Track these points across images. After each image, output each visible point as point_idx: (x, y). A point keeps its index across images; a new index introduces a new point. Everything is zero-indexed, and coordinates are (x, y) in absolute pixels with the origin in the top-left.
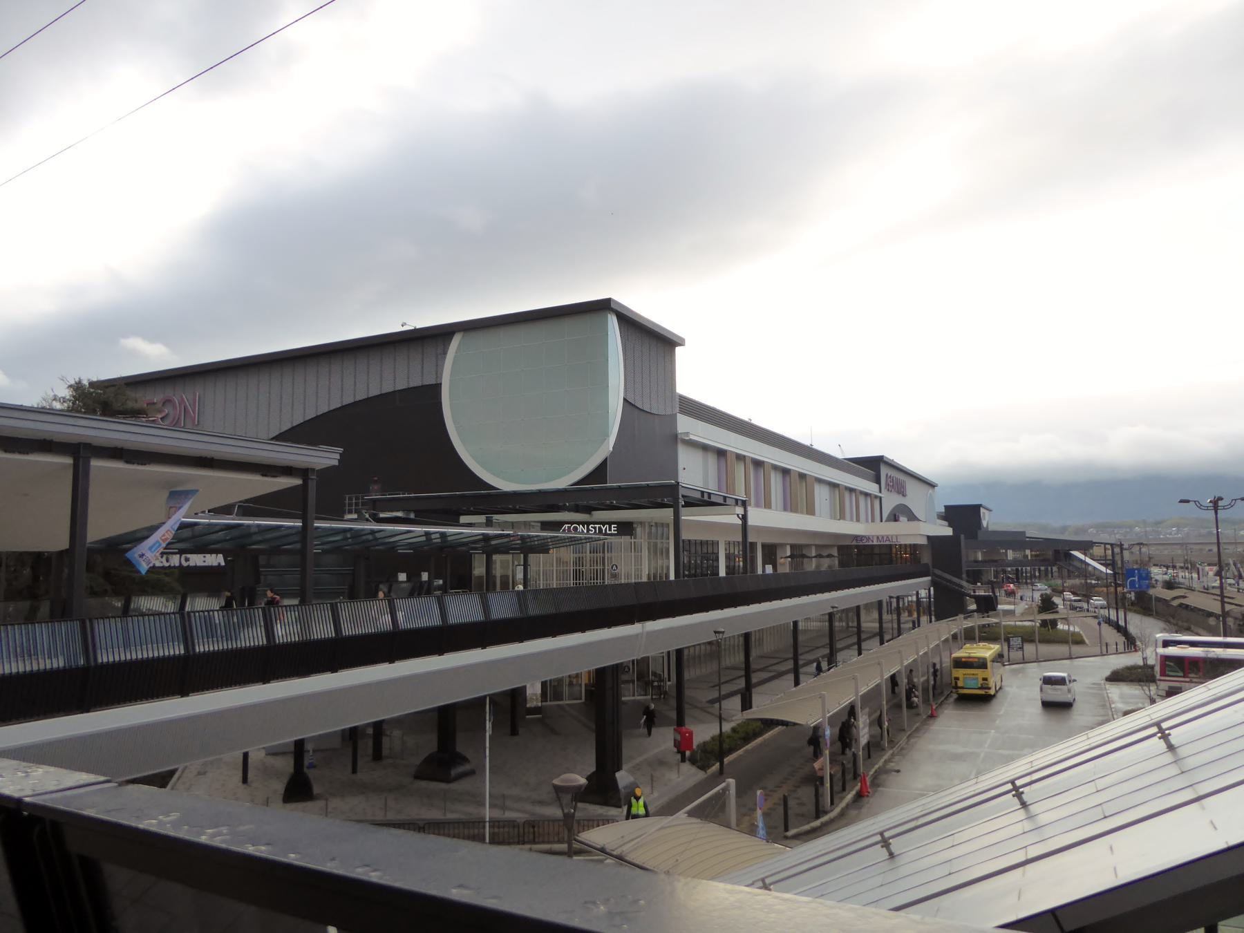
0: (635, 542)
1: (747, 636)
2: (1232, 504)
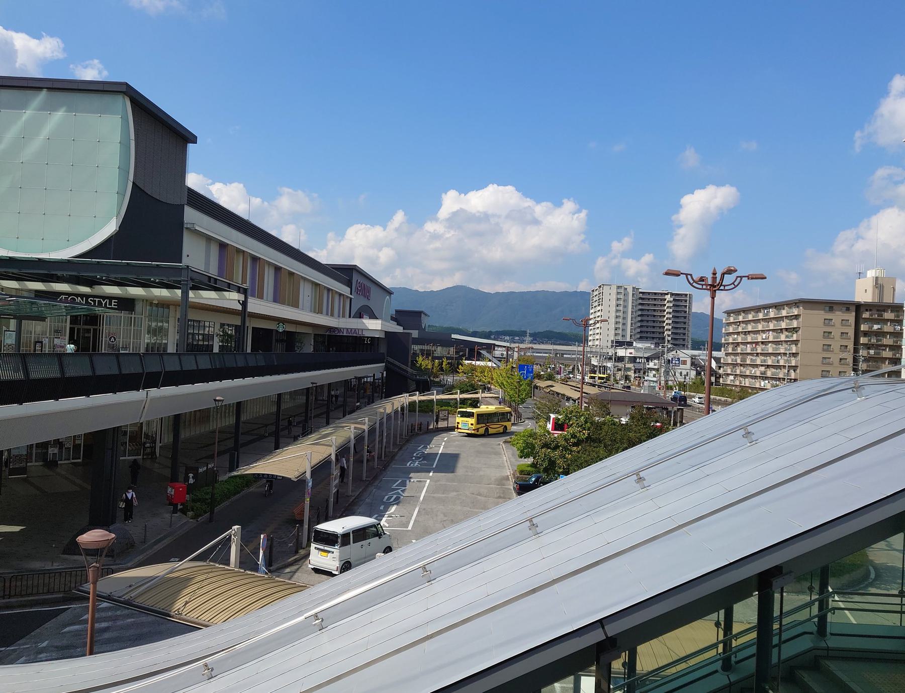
1: (239, 404)
2: (736, 284)
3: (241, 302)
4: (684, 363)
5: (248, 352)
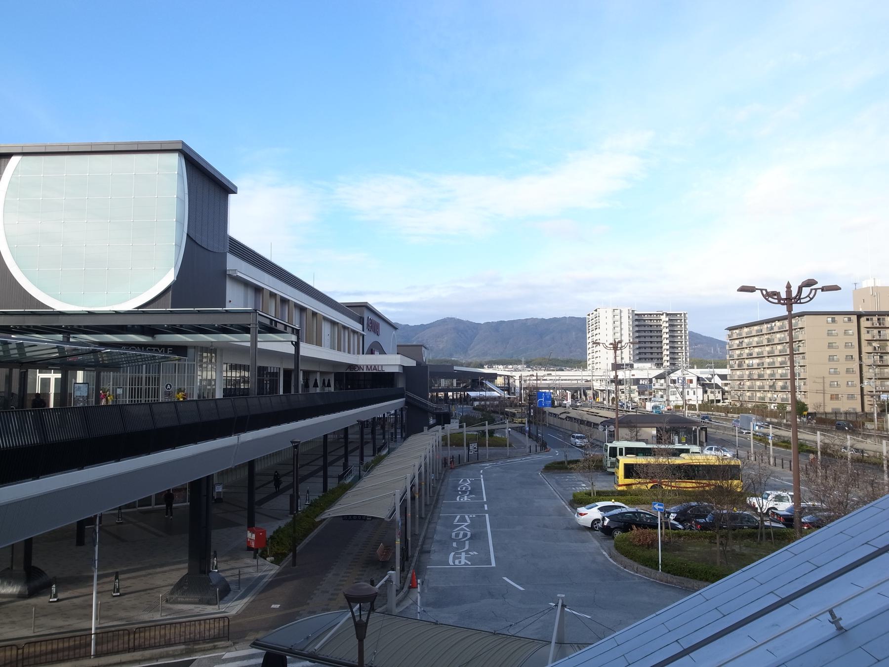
0: (179, 364)
3: (294, 343)
4: (691, 381)
5: (281, 394)
